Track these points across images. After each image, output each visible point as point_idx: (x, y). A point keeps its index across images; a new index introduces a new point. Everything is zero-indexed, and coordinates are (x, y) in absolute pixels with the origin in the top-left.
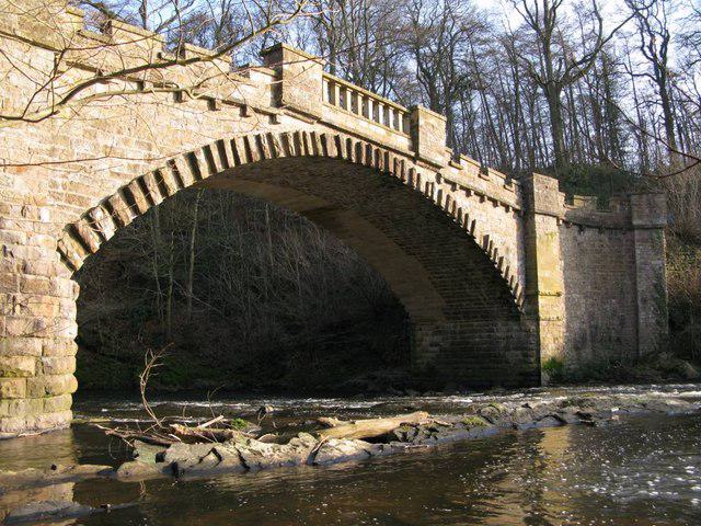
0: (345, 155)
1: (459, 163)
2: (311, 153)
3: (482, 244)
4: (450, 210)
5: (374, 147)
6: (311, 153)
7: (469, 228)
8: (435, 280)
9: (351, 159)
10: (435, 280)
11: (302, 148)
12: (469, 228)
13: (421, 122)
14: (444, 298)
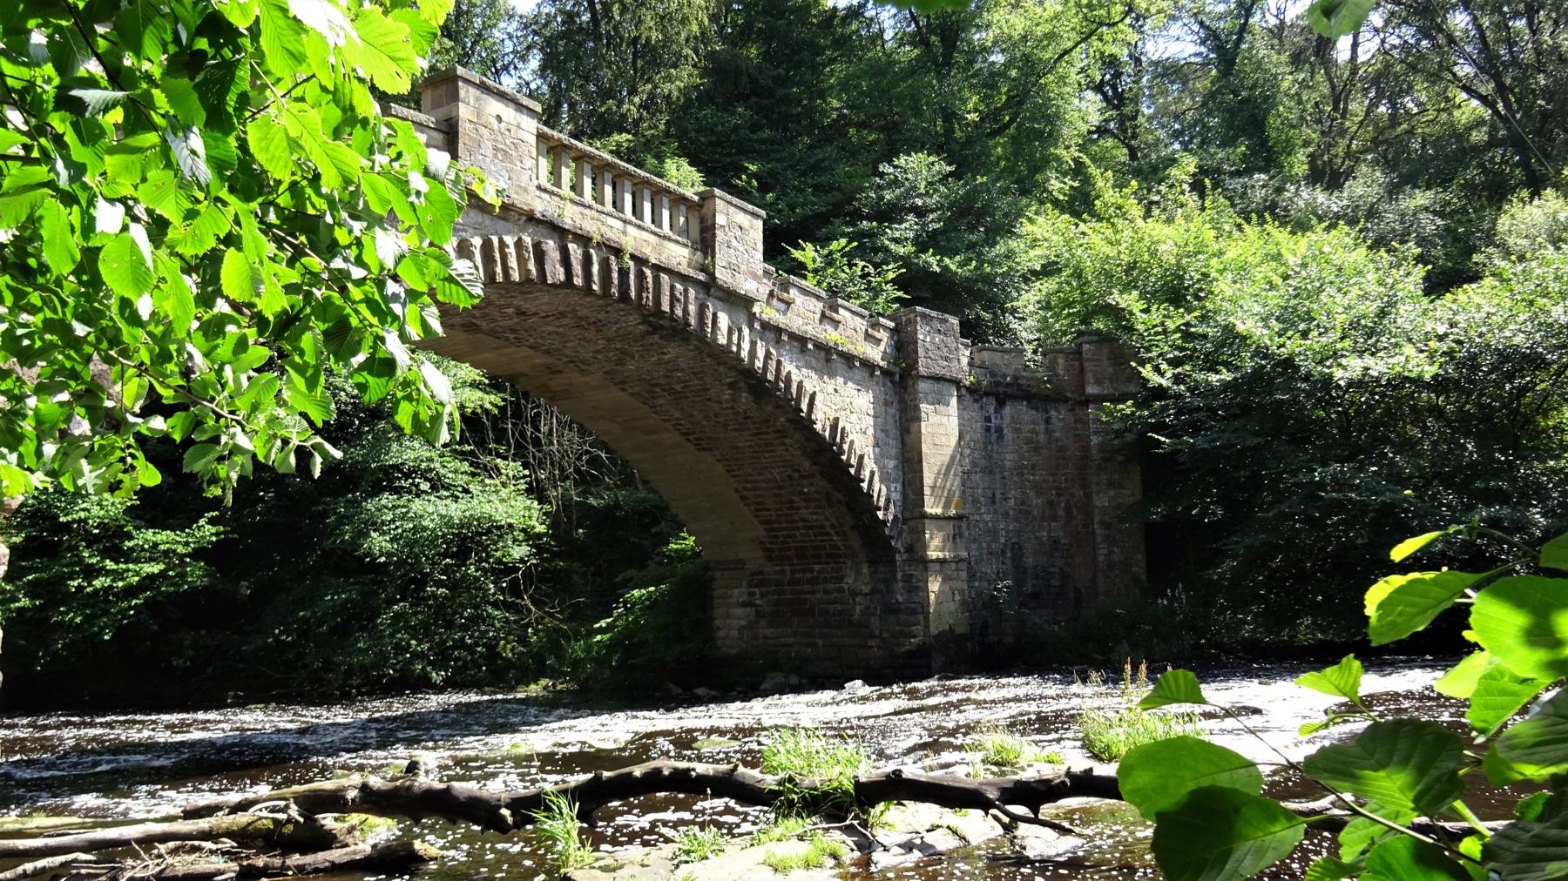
0: (578, 281)
1: (837, 312)
2: (516, 276)
3: (827, 434)
4: (770, 377)
5: (665, 278)
6: (516, 276)
7: (804, 407)
8: (746, 493)
9: (590, 288)
10: (746, 493)
11: (499, 269)
12: (804, 407)
13: (720, 219)
14: (761, 522)
